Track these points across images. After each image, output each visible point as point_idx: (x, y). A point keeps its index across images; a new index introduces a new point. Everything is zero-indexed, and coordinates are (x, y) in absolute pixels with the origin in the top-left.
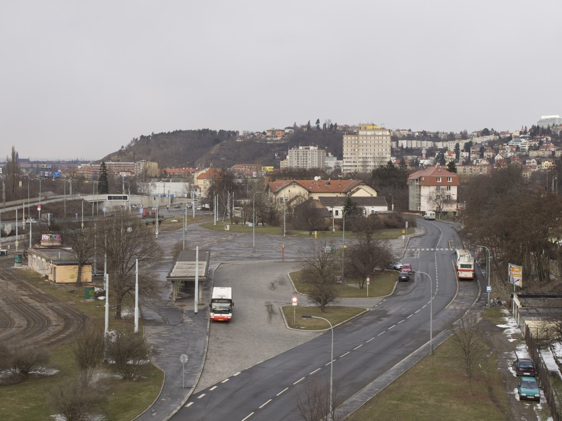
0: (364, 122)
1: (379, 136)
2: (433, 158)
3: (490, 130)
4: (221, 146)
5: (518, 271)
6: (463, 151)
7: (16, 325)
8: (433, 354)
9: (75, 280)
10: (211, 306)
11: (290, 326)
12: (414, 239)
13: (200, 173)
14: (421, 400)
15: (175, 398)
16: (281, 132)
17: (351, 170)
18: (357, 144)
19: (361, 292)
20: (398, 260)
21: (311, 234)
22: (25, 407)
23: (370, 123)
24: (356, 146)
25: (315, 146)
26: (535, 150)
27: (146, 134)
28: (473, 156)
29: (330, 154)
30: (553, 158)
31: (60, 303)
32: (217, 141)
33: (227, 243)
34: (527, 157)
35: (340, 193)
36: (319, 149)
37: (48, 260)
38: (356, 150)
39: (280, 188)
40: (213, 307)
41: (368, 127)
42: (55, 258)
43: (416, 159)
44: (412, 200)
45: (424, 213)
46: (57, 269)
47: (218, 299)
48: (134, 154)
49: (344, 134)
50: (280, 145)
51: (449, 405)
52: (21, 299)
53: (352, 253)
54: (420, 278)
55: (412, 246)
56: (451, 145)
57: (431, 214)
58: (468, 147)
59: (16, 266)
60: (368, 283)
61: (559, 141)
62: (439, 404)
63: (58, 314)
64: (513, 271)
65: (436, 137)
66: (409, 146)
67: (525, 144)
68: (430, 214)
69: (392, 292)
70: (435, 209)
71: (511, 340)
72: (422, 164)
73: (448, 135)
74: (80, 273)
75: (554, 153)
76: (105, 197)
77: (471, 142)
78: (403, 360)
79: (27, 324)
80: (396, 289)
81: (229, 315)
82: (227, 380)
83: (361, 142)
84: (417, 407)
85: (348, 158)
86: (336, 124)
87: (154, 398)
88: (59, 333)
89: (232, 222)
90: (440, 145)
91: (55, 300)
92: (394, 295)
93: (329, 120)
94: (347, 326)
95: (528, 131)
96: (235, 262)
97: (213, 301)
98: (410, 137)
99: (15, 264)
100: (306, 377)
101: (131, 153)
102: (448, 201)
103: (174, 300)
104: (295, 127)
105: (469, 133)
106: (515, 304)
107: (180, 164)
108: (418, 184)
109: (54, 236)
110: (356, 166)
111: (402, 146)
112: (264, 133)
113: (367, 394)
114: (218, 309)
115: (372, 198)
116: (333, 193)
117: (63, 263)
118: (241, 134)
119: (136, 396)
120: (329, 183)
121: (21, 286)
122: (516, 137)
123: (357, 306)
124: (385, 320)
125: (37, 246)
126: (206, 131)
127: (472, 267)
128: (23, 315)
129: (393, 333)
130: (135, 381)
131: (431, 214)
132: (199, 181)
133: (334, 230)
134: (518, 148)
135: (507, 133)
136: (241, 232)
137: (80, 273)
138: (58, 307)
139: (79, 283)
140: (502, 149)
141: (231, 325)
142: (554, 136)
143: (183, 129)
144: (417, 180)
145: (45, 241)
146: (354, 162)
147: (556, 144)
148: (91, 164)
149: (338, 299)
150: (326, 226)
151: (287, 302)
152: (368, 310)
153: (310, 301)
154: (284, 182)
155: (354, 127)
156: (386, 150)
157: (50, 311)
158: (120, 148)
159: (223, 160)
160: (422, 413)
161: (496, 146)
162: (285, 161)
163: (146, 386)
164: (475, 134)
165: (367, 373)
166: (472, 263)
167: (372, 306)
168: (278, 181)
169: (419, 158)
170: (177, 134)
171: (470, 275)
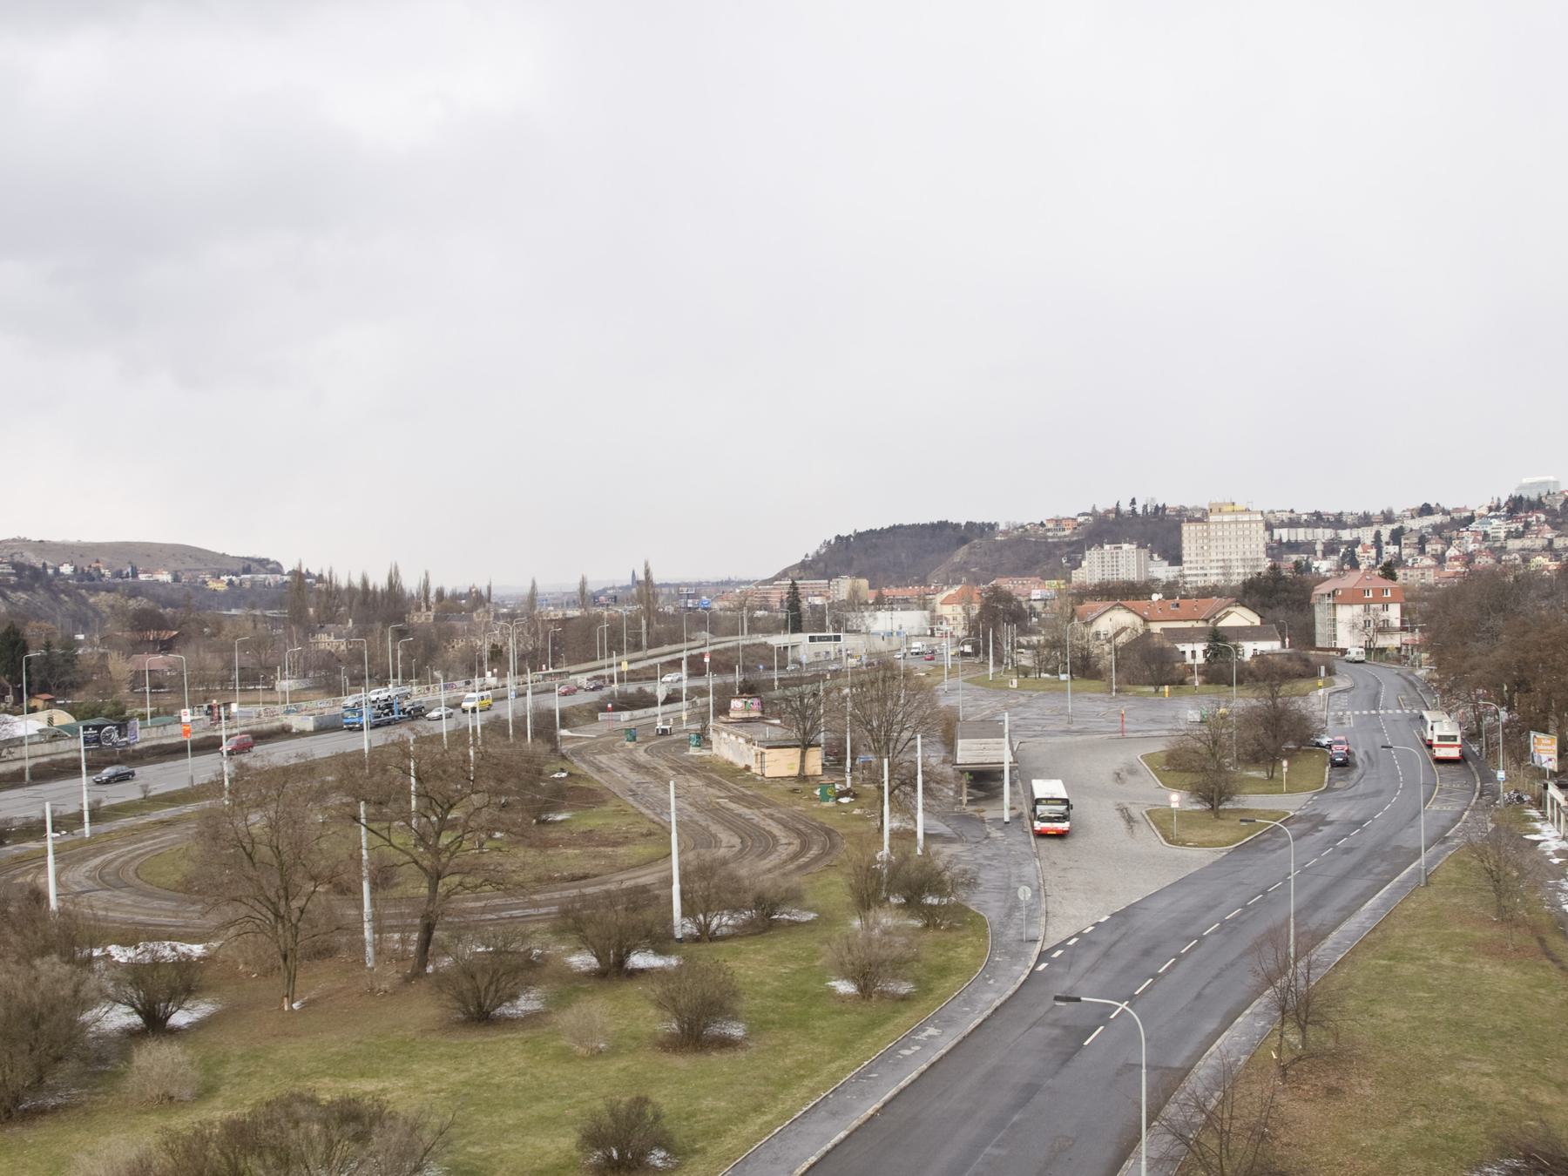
0: (1219, 500)
1: (1243, 522)
2: (1336, 558)
3: (1433, 505)
4: (971, 548)
5: (1550, 745)
6: (1388, 544)
7: (724, 844)
8: (1427, 884)
9: (795, 772)
10: (1034, 810)
11: (1170, 842)
12: (1337, 695)
13: (945, 595)
14: (1428, 959)
15: (1017, 956)
16: (1070, 522)
17: (1196, 582)
18: (1207, 537)
19: (1272, 784)
20: (1323, 731)
21: (1157, 691)
22: (783, 970)
23: (1228, 501)
24: (1206, 541)
25: (1131, 543)
26: (1516, 538)
27: (845, 534)
28: (1406, 552)
29: (1155, 556)
30: (1551, 550)
31: (782, 809)
32: (963, 541)
33: (1021, 708)
34: (1503, 549)
35: (1197, 620)
36: (1138, 548)
37: (748, 741)
38: (1205, 548)
39: (1095, 615)
40: (1038, 813)
41: (1225, 509)
42: (761, 737)
43: (1307, 560)
44: (1321, 631)
45: (1344, 651)
46: (766, 756)
47: (1047, 799)
48: (826, 566)
49: (1183, 521)
50: (1070, 544)
51: (1477, 966)
52: (718, 803)
53: (1248, 719)
54: (1366, 760)
55: (1337, 707)
56: (1367, 535)
57: (1358, 653)
58: (1396, 537)
59: (693, 751)
60: (1285, 770)
61: (1560, 520)
62: (1461, 966)
63: (785, 827)
64: (1539, 743)
65: (1338, 522)
66: (1293, 539)
67: (1498, 528)
68: (1355, 652)
69: (1325, 785)
70: (1363, 644)
71: (1556, 861)
72: (1317, 568)
73: (1360, 517)
74: (803, 761)
75: (1551, 542)
76: (802, 638)
77: (1401, 528)
78: (1377, 896)
79: (742, 842)
80: (1329, 779)
81: (1065, 826)
82: (1091, 928)
83: (1212, 534)
84: (1424, 969)
85: (1191, 562)
86: (1164, 505)
87: (982, 957)
88: (795, 856)
89: (1018, 674)
90: (1346, 535)
91: (770, 804)
92: (1328, 789)
93: (1152, 499)
94: (1265, 841)
95: (1502, 505)
96: (1042, 740)
97: (1038, 801)
98: (1293, 523)
99: (691, 748)
100: (1222, 923)
101: (821, 565)
102: (1384, 629)
103: (965, 801)
104: (1094, 513)
105: (1397, 512)
106: (1552, 799)
107: (902, 581)
108: (1331, 601)
109: (749, 701)
110: (1206, 575)
111: (1281, 539)
112: (1042, 524)
113: (1333, 949)
114: (1047, 814)
115: (1252, 628)
116: (1185, 621)
117: (776, 744)
118: (1002, 527)
119: (951, 954)
120: (1178, 605)
121: (710, 783)
122: (1481, 516)
123: (1271, 808)
124: (1326, 830)
125: (723, 718)
126: (943, 525)
127: (1459, 739)
128: (730, 828)
129: (1347, 851)
130: (944, 930)
131: (1358, 653)
132: (944, 606)
133: (1197, 684)
134: (1486, 535)
135: (1465, 509)
136: (1038, 691)
137: (803, 761)
138: (780, 815)
139: (802, 777)
140: (1458, 538)
141: (1069, 841)
142: (1551, 512)
143: (906, 523)
144: (1329, 595)
145: (735, 710)
146: (1202, 568)
147: (1555, 527)
148: (757, 586)
149: (1242, 797)
150: (1181, 677)
151: (1151, 802)
152: (1292, 814)
153: (1192, 800)
154: (1101, 605)
155: (1196, 509)
156: (1257, 545)
157: (770, 822)
158: (803, 558)
159: (974, 573)
160: (1436, 979)
161: (1446, 533)
162: (1079, 570)
163: (962, 937)
164: (1408, 514)
165: (1326, 914)
166: (1458, 733)
167: (1298, 808)
168: (1088, 604)
169: (1310, 560)
170: (895, 530)
171: (1454, 753)
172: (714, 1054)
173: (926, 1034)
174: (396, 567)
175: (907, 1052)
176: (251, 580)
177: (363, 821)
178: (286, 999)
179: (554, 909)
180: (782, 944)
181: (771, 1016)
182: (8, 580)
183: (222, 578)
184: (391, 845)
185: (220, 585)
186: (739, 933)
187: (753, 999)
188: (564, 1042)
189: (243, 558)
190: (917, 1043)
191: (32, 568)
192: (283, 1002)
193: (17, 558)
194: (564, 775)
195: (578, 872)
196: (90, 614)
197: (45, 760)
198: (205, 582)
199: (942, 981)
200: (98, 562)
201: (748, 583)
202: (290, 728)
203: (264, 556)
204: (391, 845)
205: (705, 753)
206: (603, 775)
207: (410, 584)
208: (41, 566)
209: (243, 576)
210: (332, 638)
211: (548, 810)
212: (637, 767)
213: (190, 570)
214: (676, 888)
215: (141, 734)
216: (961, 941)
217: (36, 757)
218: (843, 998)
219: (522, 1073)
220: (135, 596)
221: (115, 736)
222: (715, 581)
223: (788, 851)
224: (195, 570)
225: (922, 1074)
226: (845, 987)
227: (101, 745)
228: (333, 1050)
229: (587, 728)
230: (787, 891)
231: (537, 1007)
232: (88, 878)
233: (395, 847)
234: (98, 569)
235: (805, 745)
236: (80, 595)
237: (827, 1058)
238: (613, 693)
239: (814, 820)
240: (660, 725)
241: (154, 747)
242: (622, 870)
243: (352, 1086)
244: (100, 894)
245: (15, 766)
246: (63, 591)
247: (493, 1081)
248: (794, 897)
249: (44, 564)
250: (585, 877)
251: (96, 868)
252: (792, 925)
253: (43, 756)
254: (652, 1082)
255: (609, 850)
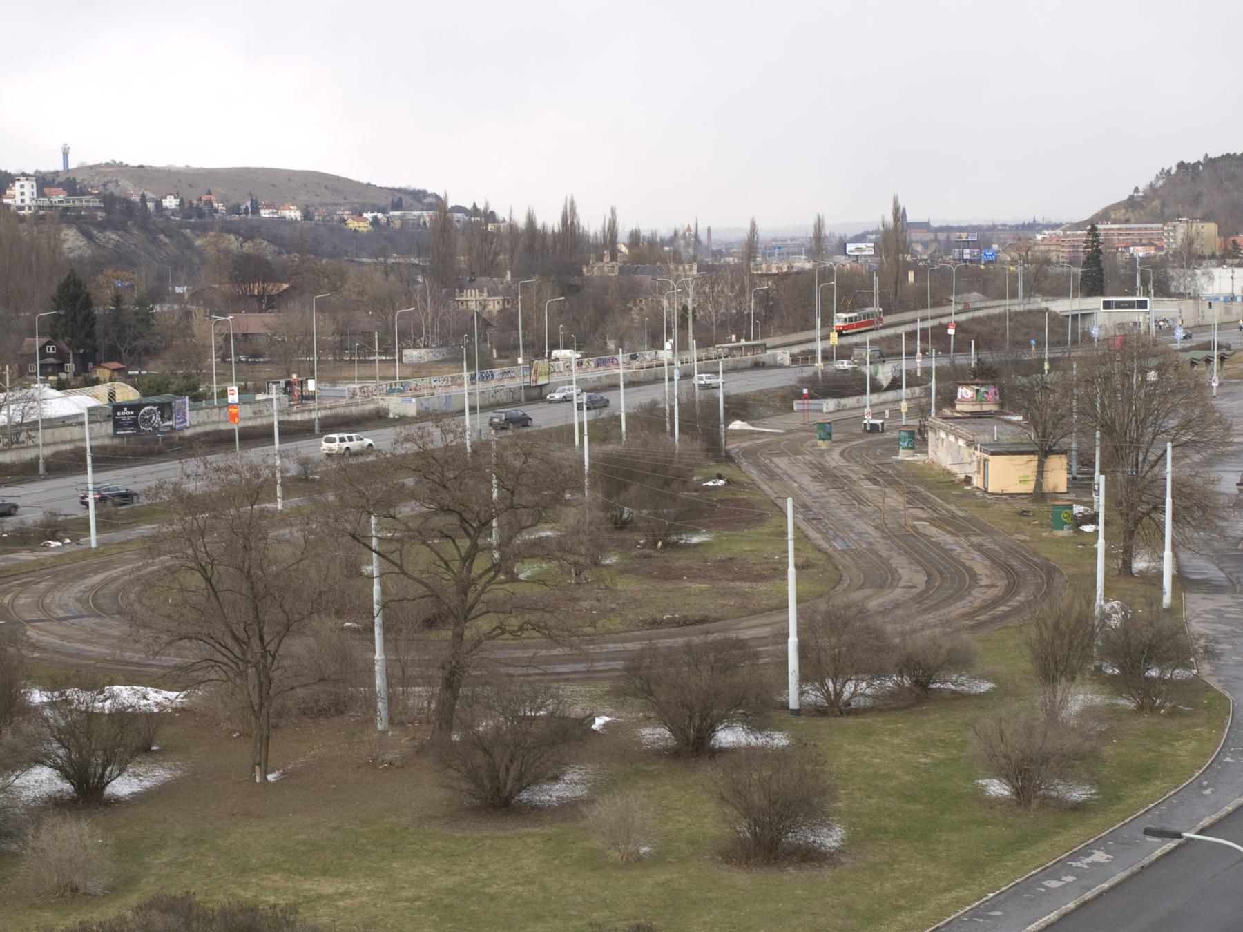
7: (902, 583)
9: (1029, 487)
22: (923, 760)
27: (1191, 159)
37: (970, 444)
42: (986, 438)
48: (1163, 204)
52: (914, 527)
59: (903, 455)
63: (994, 562)
87: (1207, 756)
88: (995, 602)
91: (985, 531)
99: (901, 451)
101: (1157, 203)
109: (983, 389)
119: (1165, 749)
121: (914, 498)
128: (919, 562)
130: (1164, 716)
138: (992, 546)
139: (1039, 495)
145: (963, 401)
148: (1064, 231)
157: (975, 554)
158: (1131, 193)
163: (1188, 727)
172: (791, 870)
173: (1089, 860)
174: (572, 203)
175: (1054, 884)
176: (401, 218)
177: (374, 542)
178: (257, 768)
179: (618, 665)
180: (933, 724)
181: (886, 822)
182: (95, 217)
183: (365, 215)
184: (404, 573)
185: (361, 225)
186: (885, 706)
187: (869, 797)
188: (596, 843)
189: (394, 189)
190: (1072, 870)
191: (126, 201)
192: (254, 771)
193: (111, 187)
194: (721, 482)
195: (694, 613)
196: (196, 260)
197: (68, 447)
198: (344, 221)
199: (1141, 786)
200: (209, 193)
201: (1055, 226)
202: (387, 412)
203: (419, 187)
204: (404, 573)
205: (919, 458)
206: (774, 485)
207: (592, 224)
208: (138, 199)
209: (392, 213)
210: (485, 294)
211: (679, 531)
212: (824, 474)
213: (326, 205)
214: (793, 640)
215: (191, 417)
216: (1184, 732)
217: (55, 443)
218: (993, 803)
219: (529, 881)
220: (251, 238)
221: (156, 419)
222: (1014, 223)
223: (985, 597)
224: (335, 204)
225: (1065, 916)
226: (997, 788)
227: (139, 430)
228: (299, 837)
229: (775, 421)
230: (949, 651)
231: (579, 793)
232: (78, 600)
233: (411, 577)
234: (209, 203)
235: (1044, 452)
236: (183, 235)
237: (942, 885)
238: (816, 373)
239: (1036, 554)
240: (868, 420)
241: (207, 434)
242: (754, 613)
243: (307, 887)
244: (86, 621)
245: (28, 455)
246: (162, 231)
247: (487, 890)
248: (959, 661)
249: (143, 197)
250: (703, 621)
251: (92, 587)
252: (957, 699)
253: (65, 442)
254: (694, 903)
255: (746, 586)
